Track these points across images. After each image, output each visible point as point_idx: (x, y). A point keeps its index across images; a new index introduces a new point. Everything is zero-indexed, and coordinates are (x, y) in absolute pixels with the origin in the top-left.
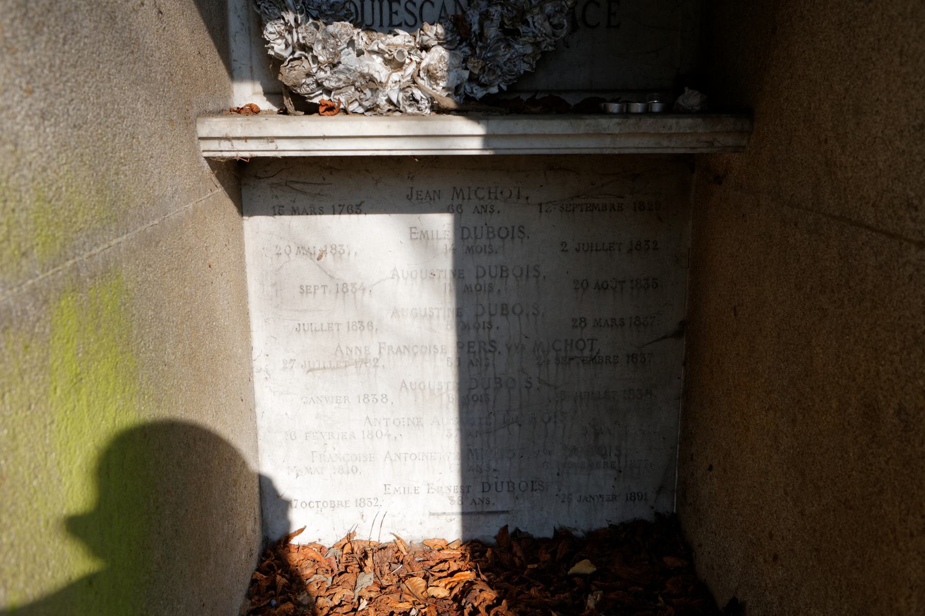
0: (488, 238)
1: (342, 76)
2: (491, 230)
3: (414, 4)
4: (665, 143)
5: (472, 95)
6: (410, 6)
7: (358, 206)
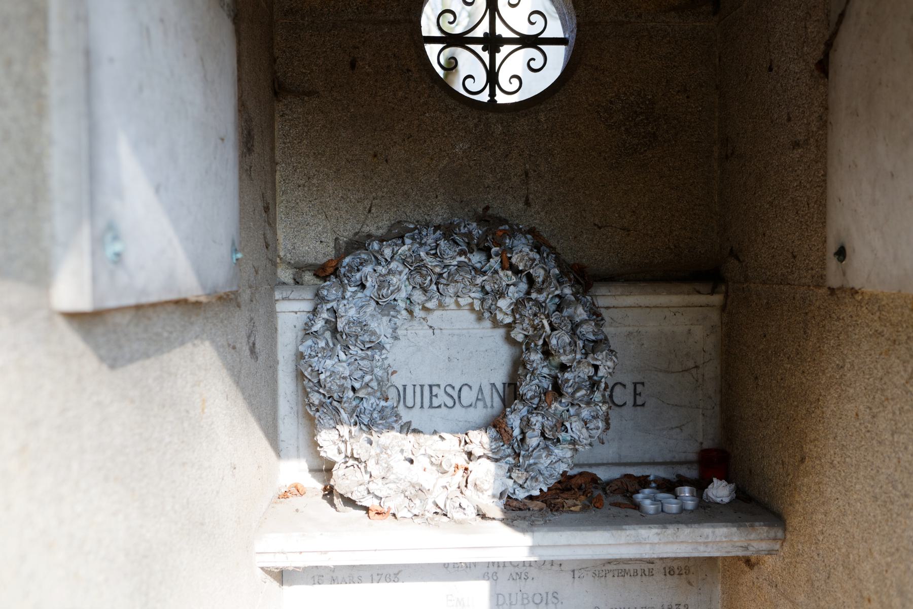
0: (523, 604)
1: (392, 486)
2: (525, 596)
3: (453, 388)
4: (702, 548)
5: (514, 497)
6: (449, 390)
7: (396, 575)
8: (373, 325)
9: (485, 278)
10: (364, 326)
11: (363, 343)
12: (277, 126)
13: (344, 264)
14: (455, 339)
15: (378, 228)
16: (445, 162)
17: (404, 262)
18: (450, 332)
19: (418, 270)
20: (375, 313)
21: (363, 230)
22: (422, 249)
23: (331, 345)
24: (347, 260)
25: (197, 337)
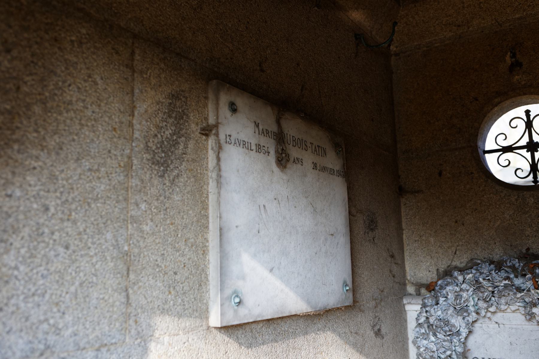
8: (453, 321)
9: (522, 294)
10: (447, 323)
11: (445, 332)
12: (403, 210)
13: (438, 284)
14: (514, 331)
15: (461, 263)
16: (499, 223)
17: (470, 284)
18: (510, 326)
19: (478, 288)
20: (453, 314)
21: (452, 264)
22: (481, 276)
23: (428, 332)
24: (439, 282)
25: (318, 330)
